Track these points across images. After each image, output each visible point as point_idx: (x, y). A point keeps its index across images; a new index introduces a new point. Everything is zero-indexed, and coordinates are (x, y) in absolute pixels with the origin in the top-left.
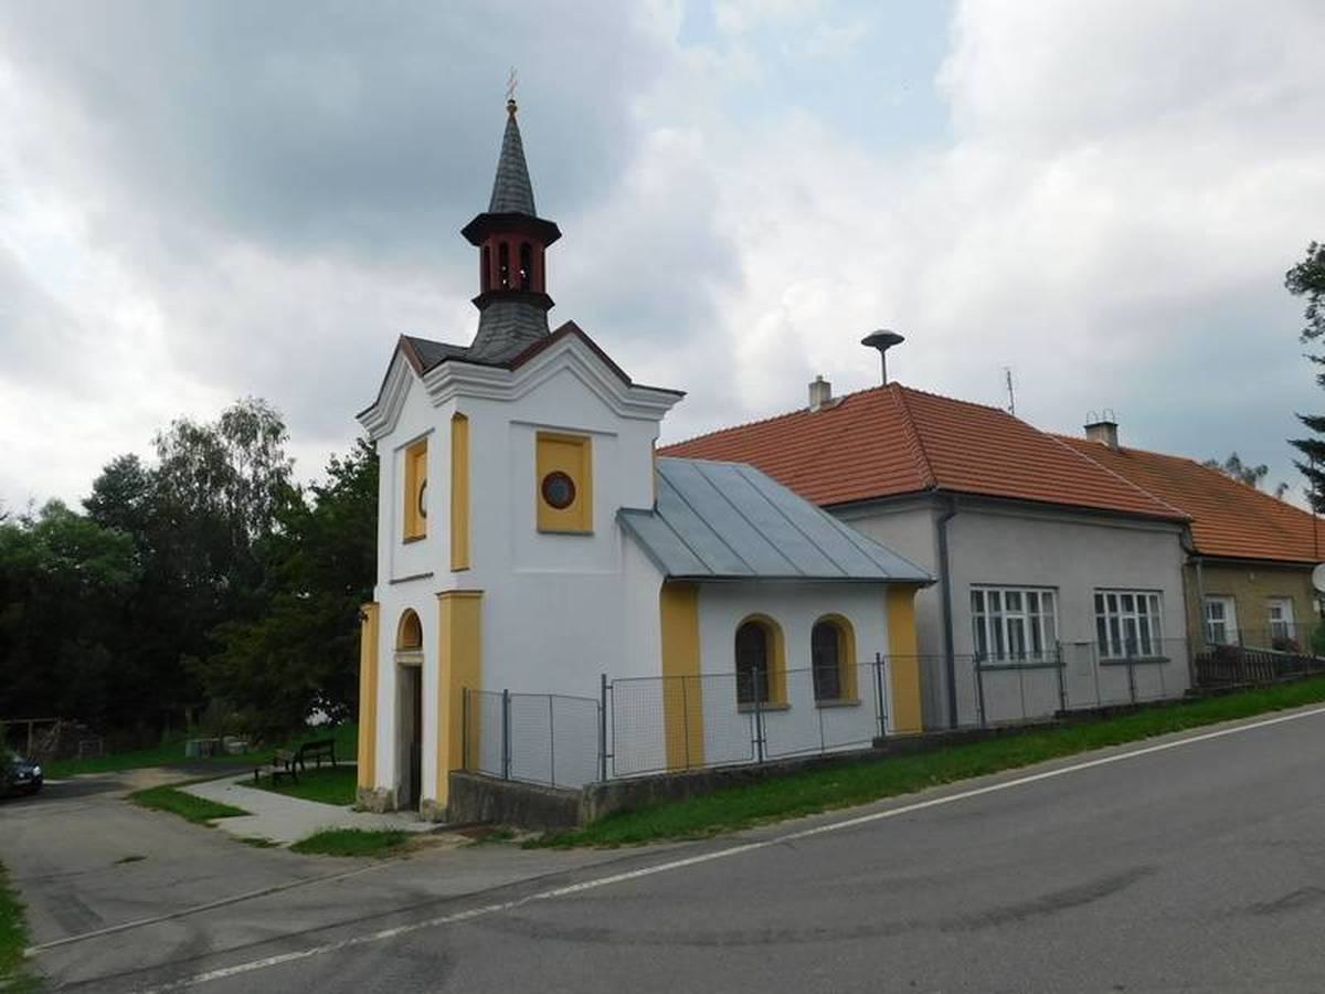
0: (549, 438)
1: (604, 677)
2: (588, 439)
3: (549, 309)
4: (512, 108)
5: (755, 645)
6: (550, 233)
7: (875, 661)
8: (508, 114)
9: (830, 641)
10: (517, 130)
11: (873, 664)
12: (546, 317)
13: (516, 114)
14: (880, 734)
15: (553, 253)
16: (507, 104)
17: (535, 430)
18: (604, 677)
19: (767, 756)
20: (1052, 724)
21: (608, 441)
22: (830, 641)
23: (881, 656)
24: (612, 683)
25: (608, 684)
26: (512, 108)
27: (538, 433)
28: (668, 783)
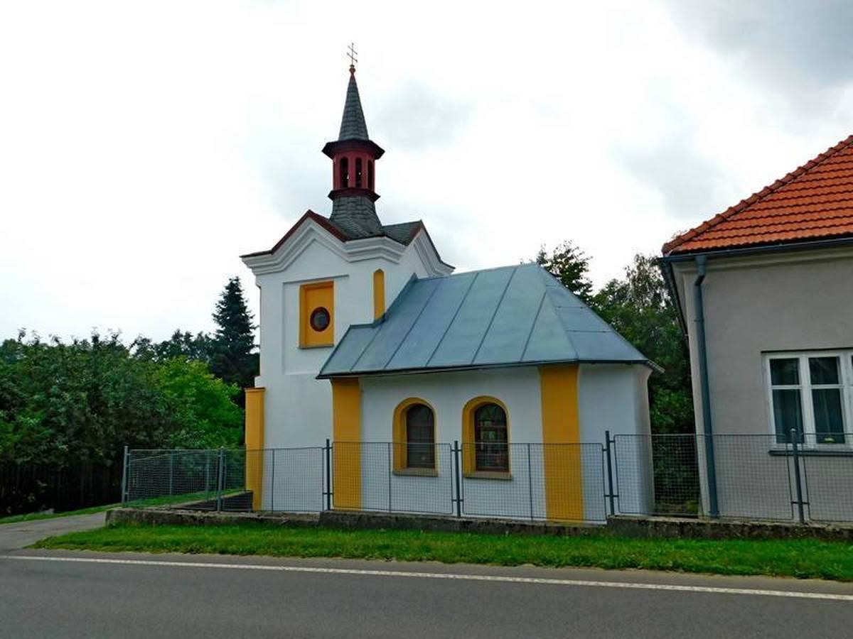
0: (309, 288)
1: (607, 433)
2: (332, 282)
3: (375, 200)
4: (352, 70)
5: (417, 421)
6: (378, 152)
7: (325, 446)
8: (350, 74)
9: (488, 423)
10: (355, 84)
11: (323, 449)
12: (374, 207)
13: (355, 74)
14: (326, 508)
15: (378, 164)
16: (350, 68)
17: (299, 284)
18: (607, 433)
19: (334, 506)
20: (643, 523)
21: (343, 281)
22: (488, 423)
23: (330, 443)
24: (614, 438)
25: (611, 439)
26: (352, 70)
27: (301, 286)
28: (144, 515)
